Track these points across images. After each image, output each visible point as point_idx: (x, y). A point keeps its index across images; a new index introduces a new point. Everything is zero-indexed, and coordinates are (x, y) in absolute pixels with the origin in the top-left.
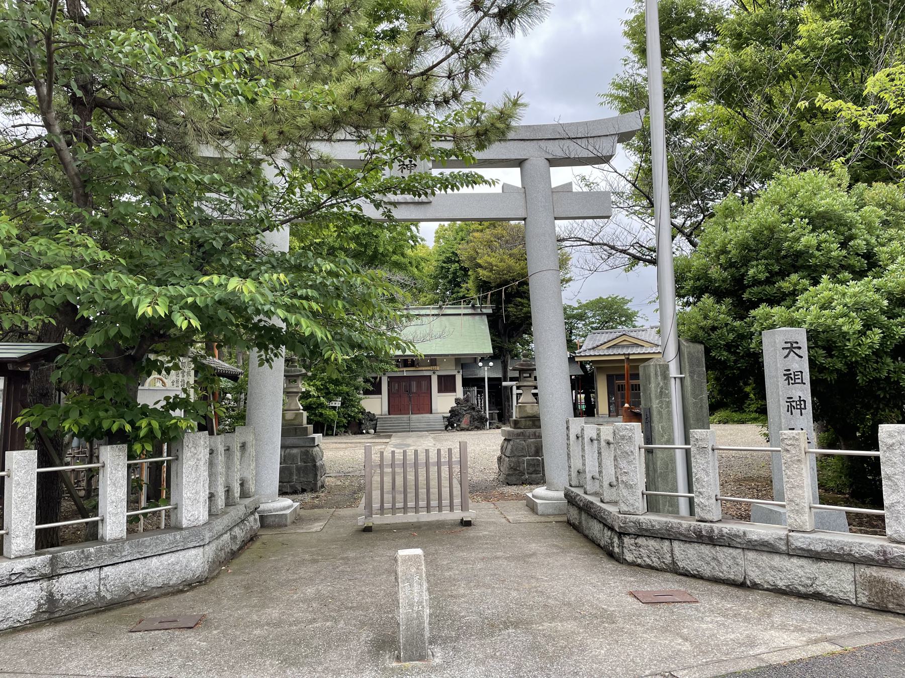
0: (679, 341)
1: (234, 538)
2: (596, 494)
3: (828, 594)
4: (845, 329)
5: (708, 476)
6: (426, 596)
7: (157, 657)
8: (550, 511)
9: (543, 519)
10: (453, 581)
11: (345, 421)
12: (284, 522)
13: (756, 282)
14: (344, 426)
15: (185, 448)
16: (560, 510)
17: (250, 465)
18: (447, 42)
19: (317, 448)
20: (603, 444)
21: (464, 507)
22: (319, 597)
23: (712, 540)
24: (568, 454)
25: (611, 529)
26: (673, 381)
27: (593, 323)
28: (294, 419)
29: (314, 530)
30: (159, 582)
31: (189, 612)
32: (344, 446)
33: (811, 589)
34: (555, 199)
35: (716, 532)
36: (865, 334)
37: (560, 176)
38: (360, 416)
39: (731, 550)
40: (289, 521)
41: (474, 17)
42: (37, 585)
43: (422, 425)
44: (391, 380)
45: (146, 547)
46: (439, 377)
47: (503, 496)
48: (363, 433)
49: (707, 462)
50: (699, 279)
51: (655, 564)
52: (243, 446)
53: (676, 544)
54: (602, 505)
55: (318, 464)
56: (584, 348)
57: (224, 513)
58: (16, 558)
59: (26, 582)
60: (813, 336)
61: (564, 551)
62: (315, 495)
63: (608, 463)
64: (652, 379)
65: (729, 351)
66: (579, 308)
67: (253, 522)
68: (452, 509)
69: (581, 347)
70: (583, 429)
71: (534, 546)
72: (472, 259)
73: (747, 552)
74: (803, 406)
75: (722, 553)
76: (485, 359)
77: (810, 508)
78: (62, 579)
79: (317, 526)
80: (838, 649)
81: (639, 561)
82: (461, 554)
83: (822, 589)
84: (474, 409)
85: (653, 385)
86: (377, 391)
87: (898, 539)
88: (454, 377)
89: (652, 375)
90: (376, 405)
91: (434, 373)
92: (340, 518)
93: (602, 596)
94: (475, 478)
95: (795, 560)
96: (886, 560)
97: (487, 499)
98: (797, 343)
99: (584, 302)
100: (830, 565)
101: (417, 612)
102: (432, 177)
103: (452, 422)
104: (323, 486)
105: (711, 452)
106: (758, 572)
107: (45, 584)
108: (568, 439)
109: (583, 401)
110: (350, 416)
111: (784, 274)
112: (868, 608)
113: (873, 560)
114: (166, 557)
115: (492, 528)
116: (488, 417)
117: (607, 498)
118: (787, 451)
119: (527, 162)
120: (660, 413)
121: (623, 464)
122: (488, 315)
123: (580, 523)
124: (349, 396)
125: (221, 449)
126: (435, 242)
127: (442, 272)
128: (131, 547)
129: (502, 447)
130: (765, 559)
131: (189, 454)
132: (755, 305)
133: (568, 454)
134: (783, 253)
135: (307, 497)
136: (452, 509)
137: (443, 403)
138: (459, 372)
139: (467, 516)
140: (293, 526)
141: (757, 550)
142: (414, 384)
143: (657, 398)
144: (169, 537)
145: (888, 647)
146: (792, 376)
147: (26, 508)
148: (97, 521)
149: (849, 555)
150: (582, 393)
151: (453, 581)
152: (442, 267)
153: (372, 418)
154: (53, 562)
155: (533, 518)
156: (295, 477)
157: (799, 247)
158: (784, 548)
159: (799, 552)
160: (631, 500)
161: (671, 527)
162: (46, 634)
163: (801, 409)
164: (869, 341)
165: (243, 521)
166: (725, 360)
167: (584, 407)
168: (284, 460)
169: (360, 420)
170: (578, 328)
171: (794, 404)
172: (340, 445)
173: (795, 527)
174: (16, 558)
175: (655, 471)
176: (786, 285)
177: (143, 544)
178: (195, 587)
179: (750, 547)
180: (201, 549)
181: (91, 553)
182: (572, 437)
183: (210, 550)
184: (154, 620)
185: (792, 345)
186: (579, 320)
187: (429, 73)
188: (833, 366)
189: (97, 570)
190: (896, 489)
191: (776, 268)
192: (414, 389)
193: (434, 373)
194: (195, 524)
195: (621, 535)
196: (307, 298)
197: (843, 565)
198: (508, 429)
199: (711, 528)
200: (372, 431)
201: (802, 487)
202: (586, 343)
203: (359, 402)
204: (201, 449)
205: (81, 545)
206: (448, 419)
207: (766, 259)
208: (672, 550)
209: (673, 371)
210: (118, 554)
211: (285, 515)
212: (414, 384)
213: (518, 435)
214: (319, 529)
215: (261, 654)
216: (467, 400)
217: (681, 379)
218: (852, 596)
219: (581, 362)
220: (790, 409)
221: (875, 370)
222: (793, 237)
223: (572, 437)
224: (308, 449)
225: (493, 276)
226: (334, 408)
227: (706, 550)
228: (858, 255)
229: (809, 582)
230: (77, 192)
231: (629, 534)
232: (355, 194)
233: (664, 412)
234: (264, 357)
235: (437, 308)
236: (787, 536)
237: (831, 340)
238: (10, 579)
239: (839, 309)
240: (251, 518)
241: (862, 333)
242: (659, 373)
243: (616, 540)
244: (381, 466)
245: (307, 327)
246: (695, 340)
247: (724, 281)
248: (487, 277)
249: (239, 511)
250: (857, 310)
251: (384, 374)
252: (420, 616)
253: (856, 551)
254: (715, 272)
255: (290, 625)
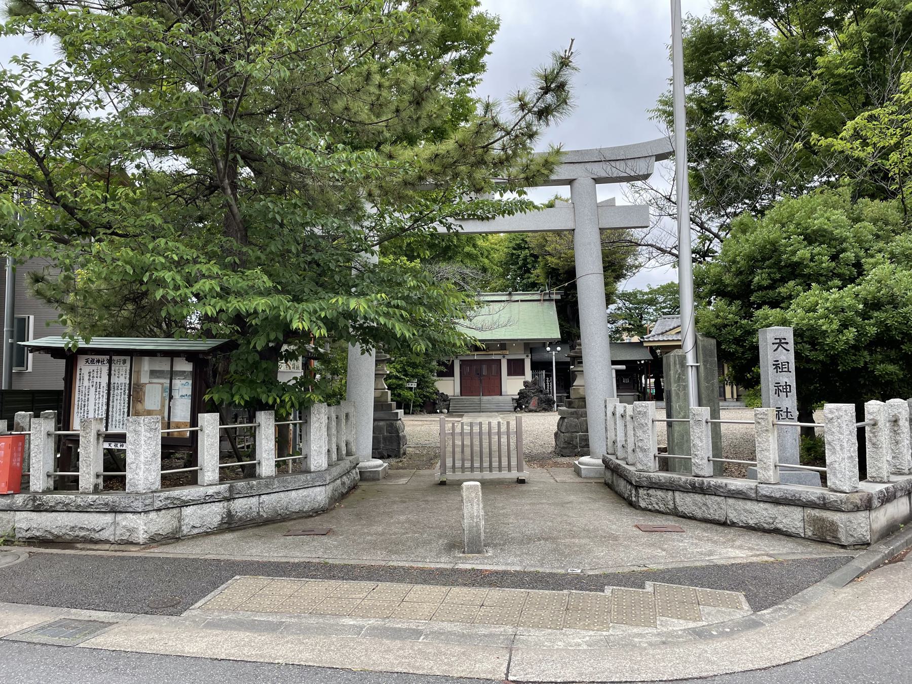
0: (696, 336)
1: (343, 484)
2: (624, 459)
3: (785, 529)
4: (824, 328)
5: (702, 442)
6: (482, 513)
7: (306, 548)
8: (592, 475)
9: (585, 480)
10: (505, 515)
11: (421, 400)
12: (377, 477)
13: (761, 288)
14: (420, 406)
15: (312, 416)
16: (600, 474)
17: (351, 431)
18: (502, 129)
19: (400, 422)
20: (628, 418)
21: (520, 469)
22: (408, 521)
23: (702, 490)
24: (606, 428)
25: (631, 484)
26: (690, 368)
27: (664, 308)
28: (381, 397)
29: (401, 483)
30: (297, 508)
31: (320, 527)
32: (420, 423)
33: (772, 526)
34: (600, 212)
35: (706, 484)
36: (842, 332)
37: (604, 193)
38: (435, 396)
39: (717, 498)
40: (381, 476)
41: (520, 114)
42: (221, 504)
43: (493, 407)
44: (463, 363)
45: (288, 483)
46: (509, 361)
47: (556, 465)
48: (437, 413)
49: (701, 432)
50: (715, 284)
51: (662, 509)
52: (347, 415)
53: (677, 494)
54: (627, 467)
55: (401, 434)
56: (653, 333)
57: (336, 465)
58: (208, 485)
59: (214, 502)
60: (799, 334)
61: (595, 500)
62: (399, 460)
63: (630, 432)
64: (672, 367)
65: (738, 344)
66: (650, 293)
67: (355, 474)
68: (509, 470)
69: (650, 331)
70: (615, 407)
71: (572, 498)
72: (542, 246)
73: (728, 499)
74: (788, 390)
75: (711, 500)
76: (553, 343)
77: (776, 466)
78: (236, 501)
79: (403, 481)
80: (772, 559)
81: (650, 507)
82: (514, 500)
83: (780, 526)
84: (541, 391)
85: (672, 372)
86: (451, 374)
87: (835, 488)
88: (523, 360)
89: (672, 364)
90: (449, 387)
91: (504, 357)
92: (420, 476)
93: (614, 527)
94: (534, 451)
95: (761, 505)
96: (825, 504)
97: (542, 466)
98: (785, 339)
99: (656, 288)
100: (786, 508)
101: (476, 523)
102: (492, 204)
103: (521, 403)
104: (404, 454)
105: (704, 424)
106: (735, 514)
107: (226, 504)
108: (606, 415)
109: (653, 385)
110: (425, 396)
111: (783, 281)
112: (814, 540)
113: (815, 504)
114: (301, 491)
115: (542, 486)
116: (555, 399)
117: (630, 460)
118: (759, 423)
119: (576, 181)
120: (677, 395)
121: (639, 433)
122: (557, 301)
123: (612, 482)
124: (424, 377)
125: (334, 417)
126: (513, 214)
127: (512, 259)
128: (279, 482)
129: (558, 424)
130: (741, 504)
131: (315, 419)
132: (759, 307)
133: (606, 428)
134: (783, 264)
135: (393, 461)
136: (509, 470)
137: (513, 386)
138: (527, 356)
139: (522, 475)
140: (383, 480)
141: (735, 498)
142: (484, 367)
143: (675, 383)
144: (302, 477)
145: (809, 561)
146: (780, 366)
147: (213, 452)
148: (255, 464)
149: (799, 500)
150: (652, 378)
151: (505, 515)
152: (513, 254)
153: (445, 398)
154: (231, 489)
155: (578, 480)
156: (382, 445)
157: (795, 259)
158: (754, 495)
159: (764, 499)
160: (645, 460)
161: (674, 481)
162: (228, 536)
163: (786, 392)
164: (844, 338)
165: (348, 472)
166: (734, 352)
167: (654, 391)
168: (375, 430)
169: (434, 400)
170: (648, 313)
171: (781, 388)
172: (416, 423)
173: (763, 480)
174: (208, 485)
175: (673, 441)
176: (783, 290)
177: (286, 481)
178: (320, 514)
179: (730, 495)
180: (324, 487)
181: (254, 485)
182: (609, 414)
183: (329, 488)
184: (298, 530)
185: (780, 340)
186: (649, 305)
187: (490, 146)
188: (816, 358)
189: (257, 497)
190: (834, 452)
191: (778, 276)
192: (485, 373)
193: (504, 357)
194: (319, 469)
195: (637, 487)
196: (397, 307)
197: (795, 508)
198: (564, 408)
199: (703, 481)
200: (446, 411)
201: (769, 450)
202: (655, 327)
203: (433, 384)
204: (322, 415)
205: (249, 479)
206: (517, 400)
207: (770, 268)
208: (674, 499)
209: (690, 360)
210: (271, 487)
211: (378, 471)
212: (484, 367)
213: (572, 413)
214: (404, 482)
215: (374, 548)
216: (535, 383)
217: (697, 367)
218: (801, 530)
219: (651, 347)
220: (778, 392)
221: (853, 361)
222: (791, 251)
223: (609, 414)
224: (392, 422)
225: (561, 264)
226: (411, 389)
227: (698, 498)
228: (848, 265)
229: (771, 521)
230: (241, 234)
231: (643, 487)
232: (432, 220)
233: (681, 394)
234: (364, 348)
235: (506, 295)
236: (756, 486)
237: (814, 337)
238: (205, 499)
239: (821, 311)
240: (354, 471)
241: (840, 331)
242: (677, 362)
243: (634, 492)
244: (453, 434)
245: (400, 329)
246: (708, 335)
247: (735, 286)
248: (555, 265)
249: (346, 464)
250: (836, 314)
251: (457, 358)
252: (477, 525)
253: (804, 497)
254: (727, 279)
255: (391, 535)
